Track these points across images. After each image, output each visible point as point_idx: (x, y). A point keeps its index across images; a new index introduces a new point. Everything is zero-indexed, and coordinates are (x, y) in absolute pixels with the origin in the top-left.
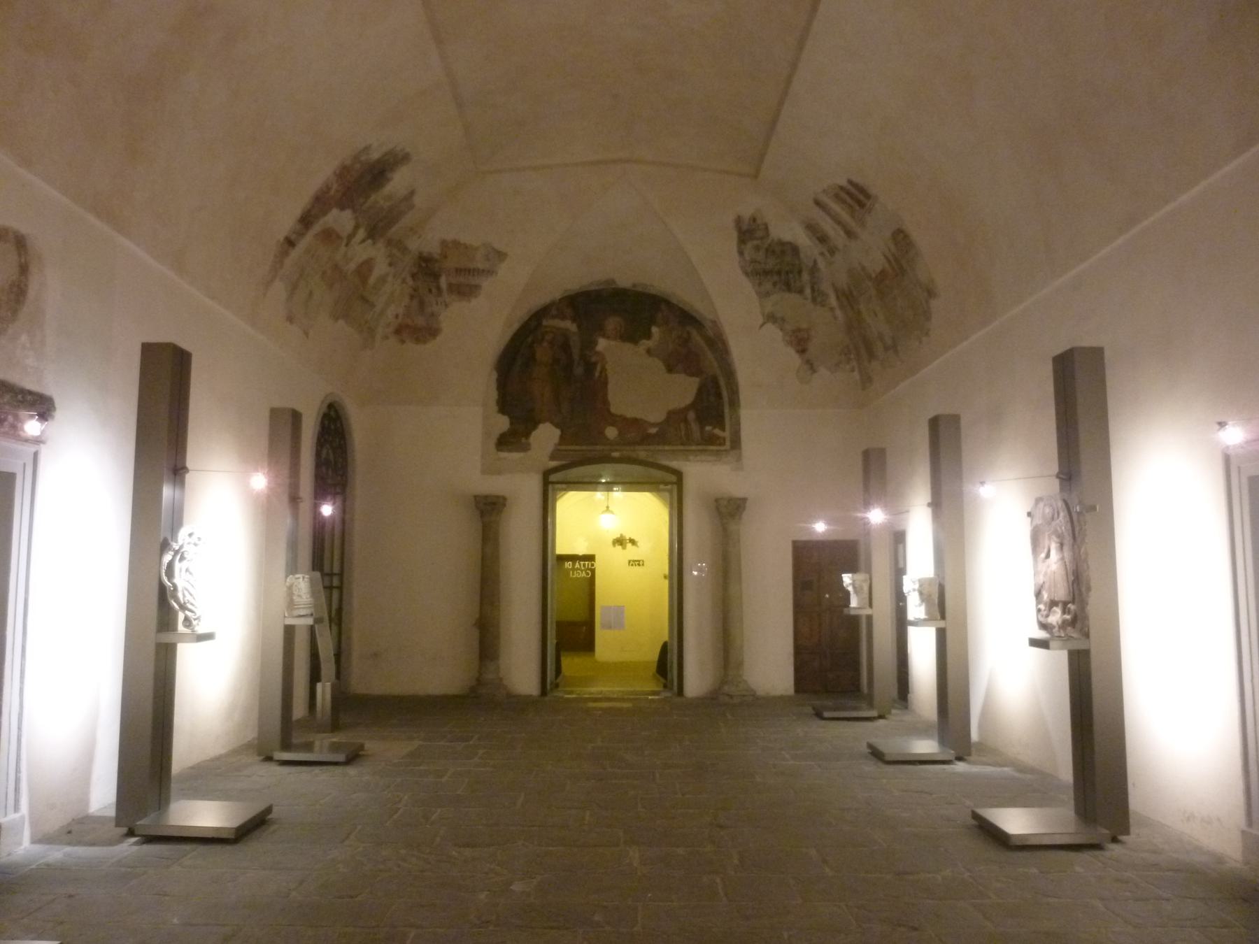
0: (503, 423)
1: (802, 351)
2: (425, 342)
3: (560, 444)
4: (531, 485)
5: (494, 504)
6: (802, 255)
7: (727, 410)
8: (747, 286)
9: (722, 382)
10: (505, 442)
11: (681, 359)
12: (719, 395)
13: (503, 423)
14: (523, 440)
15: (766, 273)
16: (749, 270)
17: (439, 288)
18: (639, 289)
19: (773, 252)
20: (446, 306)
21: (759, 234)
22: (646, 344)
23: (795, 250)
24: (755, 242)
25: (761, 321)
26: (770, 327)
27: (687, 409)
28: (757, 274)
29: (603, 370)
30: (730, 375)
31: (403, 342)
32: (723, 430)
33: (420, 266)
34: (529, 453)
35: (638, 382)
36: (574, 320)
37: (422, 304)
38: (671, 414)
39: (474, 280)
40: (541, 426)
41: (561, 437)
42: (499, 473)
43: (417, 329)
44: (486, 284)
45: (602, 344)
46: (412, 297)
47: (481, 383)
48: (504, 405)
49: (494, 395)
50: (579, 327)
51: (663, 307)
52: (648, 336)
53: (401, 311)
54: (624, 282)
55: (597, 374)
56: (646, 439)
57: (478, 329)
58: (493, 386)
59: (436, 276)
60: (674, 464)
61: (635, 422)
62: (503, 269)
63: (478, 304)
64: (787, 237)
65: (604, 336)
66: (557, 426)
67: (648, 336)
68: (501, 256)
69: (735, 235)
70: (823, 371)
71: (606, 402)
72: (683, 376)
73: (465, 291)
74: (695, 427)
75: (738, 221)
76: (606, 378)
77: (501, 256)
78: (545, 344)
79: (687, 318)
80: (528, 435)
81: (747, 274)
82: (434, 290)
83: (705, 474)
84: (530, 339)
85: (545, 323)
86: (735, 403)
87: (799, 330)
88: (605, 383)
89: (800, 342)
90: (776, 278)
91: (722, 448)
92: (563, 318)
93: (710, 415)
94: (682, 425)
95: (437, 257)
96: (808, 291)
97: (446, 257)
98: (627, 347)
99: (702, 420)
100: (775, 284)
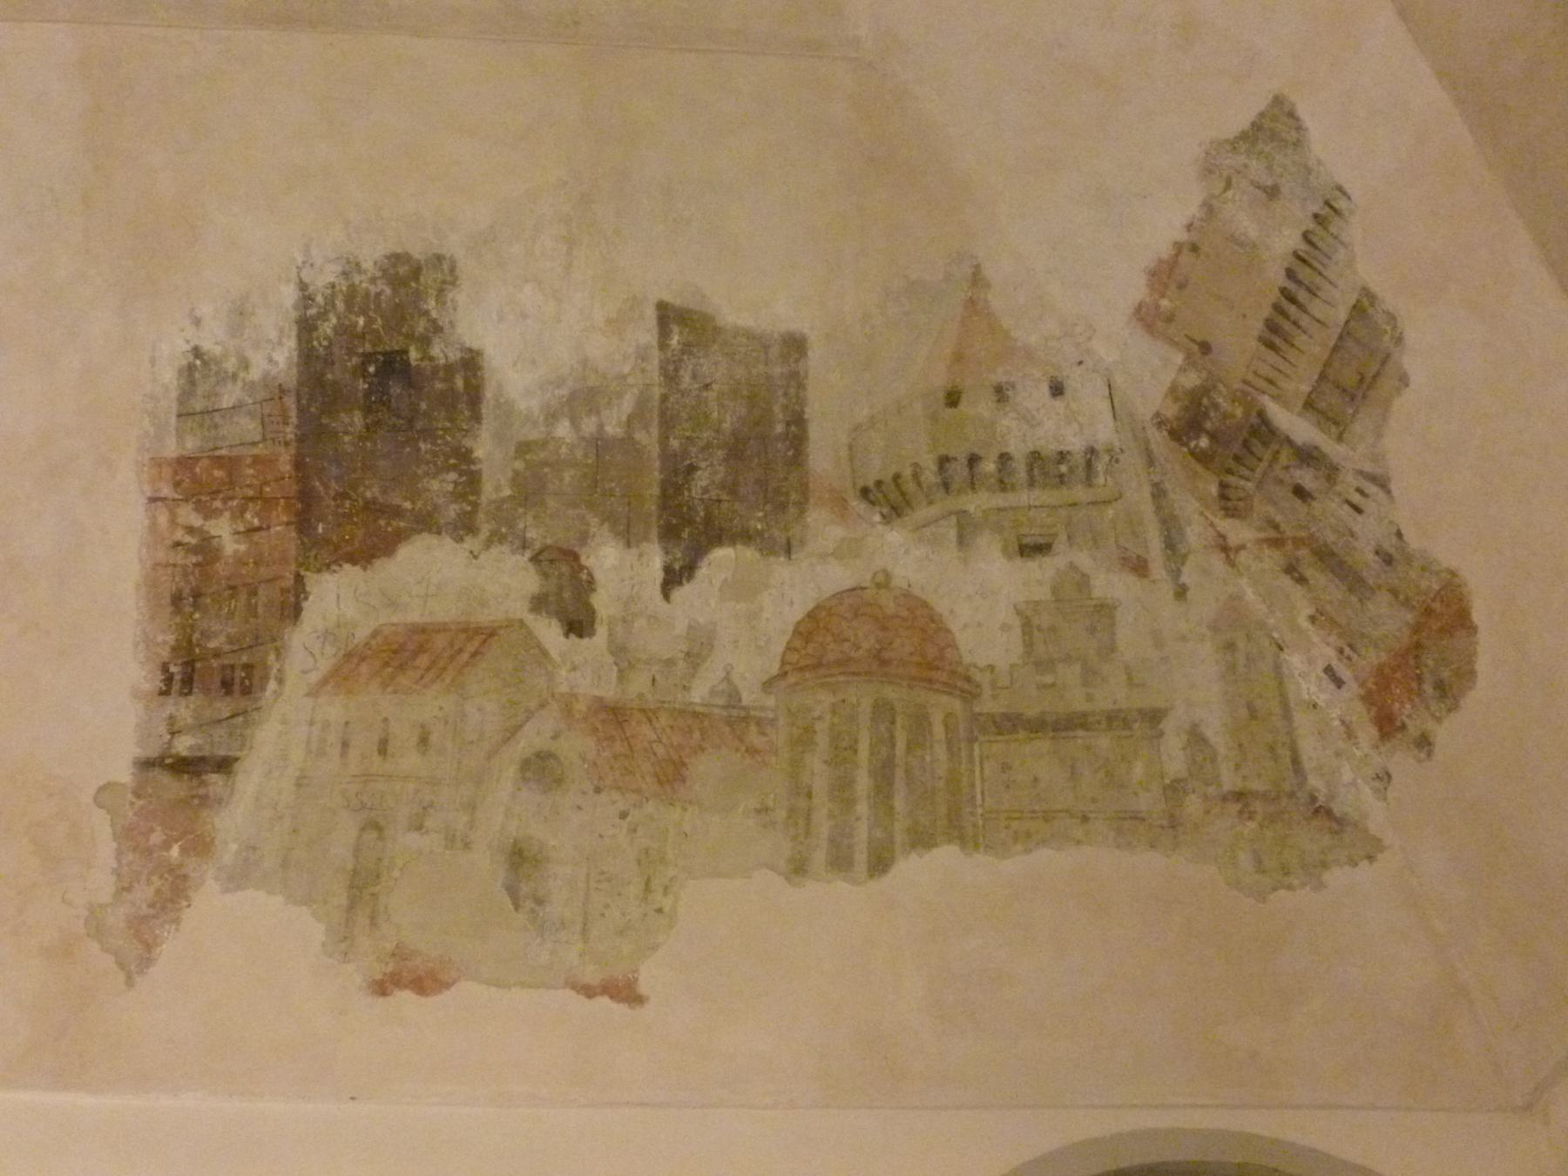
2: (1467, 675)
17: (1308, 456)
20: (1382, 483)
37: (1326, 556)
42: (798, 420)
44: (1367, 262)
59: (1263, 430)
62: (1333, 147)
63: (1435, 349)
68: (1275, 127)
73: (1359, 371)
77: (1275, 127)
82: (1307, 478)
95: (1192, 380)
97: (1205, 348)
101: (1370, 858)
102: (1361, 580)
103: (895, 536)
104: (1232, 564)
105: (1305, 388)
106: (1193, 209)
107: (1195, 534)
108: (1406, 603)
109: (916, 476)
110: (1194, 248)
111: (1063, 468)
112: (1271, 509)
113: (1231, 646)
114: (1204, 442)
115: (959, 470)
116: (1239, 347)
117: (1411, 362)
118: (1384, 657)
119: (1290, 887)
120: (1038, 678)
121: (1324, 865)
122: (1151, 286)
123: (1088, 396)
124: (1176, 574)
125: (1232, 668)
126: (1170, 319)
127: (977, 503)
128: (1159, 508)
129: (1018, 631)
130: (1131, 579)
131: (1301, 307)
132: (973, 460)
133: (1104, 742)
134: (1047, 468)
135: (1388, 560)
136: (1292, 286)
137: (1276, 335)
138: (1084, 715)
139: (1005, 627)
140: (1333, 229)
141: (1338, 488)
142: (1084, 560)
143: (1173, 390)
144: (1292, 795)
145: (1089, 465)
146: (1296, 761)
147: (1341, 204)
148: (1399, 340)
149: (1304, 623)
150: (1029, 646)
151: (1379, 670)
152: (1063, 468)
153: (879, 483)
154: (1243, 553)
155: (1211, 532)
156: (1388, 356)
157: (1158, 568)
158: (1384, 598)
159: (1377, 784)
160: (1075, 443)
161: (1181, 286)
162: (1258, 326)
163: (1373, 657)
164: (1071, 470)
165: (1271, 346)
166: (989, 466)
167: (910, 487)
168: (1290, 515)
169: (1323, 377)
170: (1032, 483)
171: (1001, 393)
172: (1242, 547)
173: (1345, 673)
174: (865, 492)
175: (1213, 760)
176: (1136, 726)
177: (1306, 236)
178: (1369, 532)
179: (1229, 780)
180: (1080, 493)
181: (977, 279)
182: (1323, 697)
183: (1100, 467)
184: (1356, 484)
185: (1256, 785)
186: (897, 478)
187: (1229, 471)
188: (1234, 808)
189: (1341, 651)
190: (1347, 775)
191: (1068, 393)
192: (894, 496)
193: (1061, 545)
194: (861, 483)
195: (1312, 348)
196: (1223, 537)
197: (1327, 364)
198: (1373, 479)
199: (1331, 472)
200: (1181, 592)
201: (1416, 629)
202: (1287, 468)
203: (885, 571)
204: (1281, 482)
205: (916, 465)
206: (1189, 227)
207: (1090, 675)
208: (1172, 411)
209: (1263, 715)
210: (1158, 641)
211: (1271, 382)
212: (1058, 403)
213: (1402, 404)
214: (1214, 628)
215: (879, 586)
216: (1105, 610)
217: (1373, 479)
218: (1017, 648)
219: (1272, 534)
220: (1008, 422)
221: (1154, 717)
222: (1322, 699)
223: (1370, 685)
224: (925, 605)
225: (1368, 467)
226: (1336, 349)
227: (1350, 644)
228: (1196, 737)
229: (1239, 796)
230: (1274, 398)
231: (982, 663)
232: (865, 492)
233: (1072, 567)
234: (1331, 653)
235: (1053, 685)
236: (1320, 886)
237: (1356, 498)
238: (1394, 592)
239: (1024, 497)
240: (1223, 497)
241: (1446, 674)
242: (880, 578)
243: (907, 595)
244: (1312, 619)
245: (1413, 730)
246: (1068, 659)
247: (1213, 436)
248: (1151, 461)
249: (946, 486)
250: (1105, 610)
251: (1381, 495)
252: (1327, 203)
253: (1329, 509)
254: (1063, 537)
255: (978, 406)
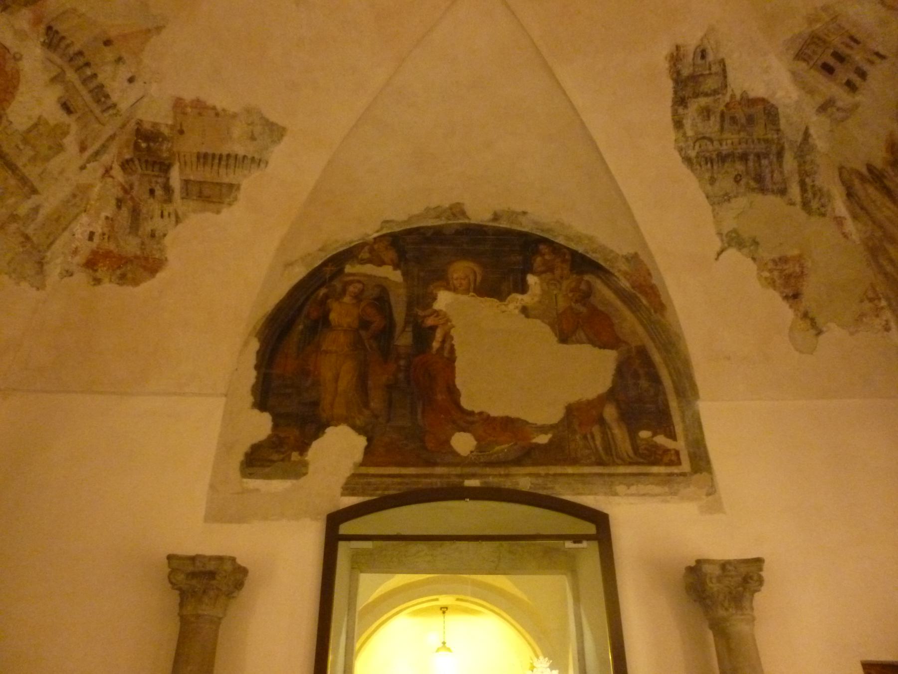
0: (260, 426)
1: (794, 297)
2: (136, 282)
3: (363, 464)
4: (302, 544)
5: (212, 575)
6: (783, 122)
7: (673, 404)
8: (691, 186)
9: (657, 358)
10: (257, 461)
11: (581, 323)
12: (656, 379)
13: (260, 426)
14: (295, 456)
15: (723, 158)
16: (692, 154)
17: (168, 189)
18: (503, 224)
19: (734, 120)
20: (178, 221)
21: (711, 84)
22: (518, 300)
23: (771, 113)
24: (703, 101)
25: (717, 244)
26: (732, 253)
27: (602, 400)
28: (706, 160)
29: (447, 337)
30: (671, 343)
31: (98, 281)
32: (673, 436)
33: (136, 146)
34: (302, 480)
35: (511, 362)
36: (396, 267)
37: (136, 214)
38: (571, 410)
39: (227, 177)
40: (330, 431)
41: (368, 451)
42: (240, 519)
43: (126, 261)
44: (248, 182)
45: (444, 300)
46: (119, 203)
47: (230, 357)
48: (264, 397)
49: (251, 376)
50: (405, 274)
51: (542, 247)
52: (523, 288)
53: (98, 229)
54: (479, 213)
55: (436, 345)
56: (529, 455)
57: (231, 265)
58: (251, 359)
59: (165, 168)
60: (589, 500)
61: (509, 425)
62: (278, 156)
63: (233, 217)
64: (758, 90)
65: (448, 288)
66: (360, 430)
67: (523, 288)
68: (276, 132)
69: (668, 86)
70: (834, 333)
71: (453, 393)
72: (587, 348)
73: (212, 195)
74: (619, 433)
75: (676, 58)
76: (452, 350)
77: (276, 132)
78: (347, 299)
79: (582, 264)
80: (303, 448)
81: (688, 160)
82: (159, 192)
83: (650, 523)
84: (323, 291)
85: (348, 269)
86: (687, 389)
87: (784, 260)
88: (451, 360)
89: (789, 280)
90: (740, 167)
91: (675, 470)
92: (381, 263)
93: (644, 415)
94: (596, 429)
95: (166, 131)
96: (795, 190)
98: (487, 306)
99: (632, 418)
100: (737, 179)
101: (38, 289)
102: (137, 230)
103: (38, 51)
104: (103, 176)
105: (192, 178)
106: (233, 109)
107: (106, 158)
108: (143, 250)
109: (68, 46)
110: (217, 115)
111: (103, 99)
112: (136, 184)
113: (74, 196)
114: (144, 145)
115: (81, 61)
116: (190, 145)
117: (226, 212)
118: (116, 251)
119: (10, 277)
120: (19, 143)
121: (25, 278)
122: (192, 101)
123: (134, 92)
124: (88, 161)
125: (68, 201)
126: (185, 114)
127: (71, 75)
128: (108, 140)
129: (31, 123)
130: (77, 149)
131: (220, 163)
132: (87, 64)
133: (12, 182)
134: (100, 94)
135: (153, 235)
136: (224, 158)
137: (204, 158)
138: (17, 168)
139: (30, 118)
140: (253, 166)
141: (165, 205)
142: (74, 128)
143: (155, 125)
144: (39, 251)
145: (109, 108)
146: (52, 243)
147: (262, 165)
148: (230, 204)
149: (103, 215)
150: (29, 131)
151: (111, 252)
152: (103, 99)
153: (57, 32)
154: (111, 179)
155: (110, 163)
156: (223, 203)
157: (87, 154)
158: (138, 241)
159: (64, 273)
160: (115, 98)
161: (200, 114)
162: (203, 150)
163: (112, 246)
164: (104, 102)
165: (198, 158)
166: (89, 72)
167: (63, 45)
168: (140, 191)
169: (200, 183)
170: (91, 91)
171: (119, 60)
172: (112, 177)
173: (96, 239)
174: (49, 28)
175: (33, 220)
176: (27, 188)
177: (245, 157)
178: (157, 224)
179: (30, 231)
180: (97, 111)
181: (159, 29)
182: (80, 236)
183: (111, 112)
184: (171, 211)
185: (35, 239)
186: (63, 38)
187: (139, 160)
188: (22, 239)
189: (104, 234)
190: (59, 261)
191: (132, 85)
192: (55, 41)
193: (74, 117)
194: (52, 24)
195: (205, 174)
196: (111, 168)
197: (204, 182)
198: (177, 217)
199: (169, 199)
200: (83, 168)
201: (136, 257)
202: (157, 182)
203: (21, 56)
204: (150, 182)
205: (72, 43)
206: (224, 110)
207: (33, 159)
208: (147, 126)
209: (60, 222)
210: (62, 172)
211: (185, 163)
212: (126, 84)
213: (209, 215)
214: (78, 187)
215: (14, 57)
216: (60, 148)
217: (177, 217)
218: (23, 128)
219: (127, 187)
220: (109, 68)
221: (34, 191)
222: (78, 236)
223: (101, 251)
224: (19, 81)
225: (180, 213)
226: (212, 183)
227: (110, 235)
228: (36, 210)
229: (27, 238)
230: (180, 168)
231: (11, 119)
232: (49, 28)
233: (69, 126)
234: (100, 231)
235: (21, 150)
236: (18, 284)
237: (166, 213)
238: (143, 243)
239: (84, 92)
240: (127, 161)
241: (130, 275)
242: (18, 56)
243: (18, 71)
244: (107, 218)
245: (99, 274)
246: (34, 147)
247: (148, 148)
248: (123, 126)
249: (71, 60)
250: (60, 148)
251: (173, 222)
252: (260, 160)
253: (153, 206)
254: (78, 115)
255: (109, 54)
